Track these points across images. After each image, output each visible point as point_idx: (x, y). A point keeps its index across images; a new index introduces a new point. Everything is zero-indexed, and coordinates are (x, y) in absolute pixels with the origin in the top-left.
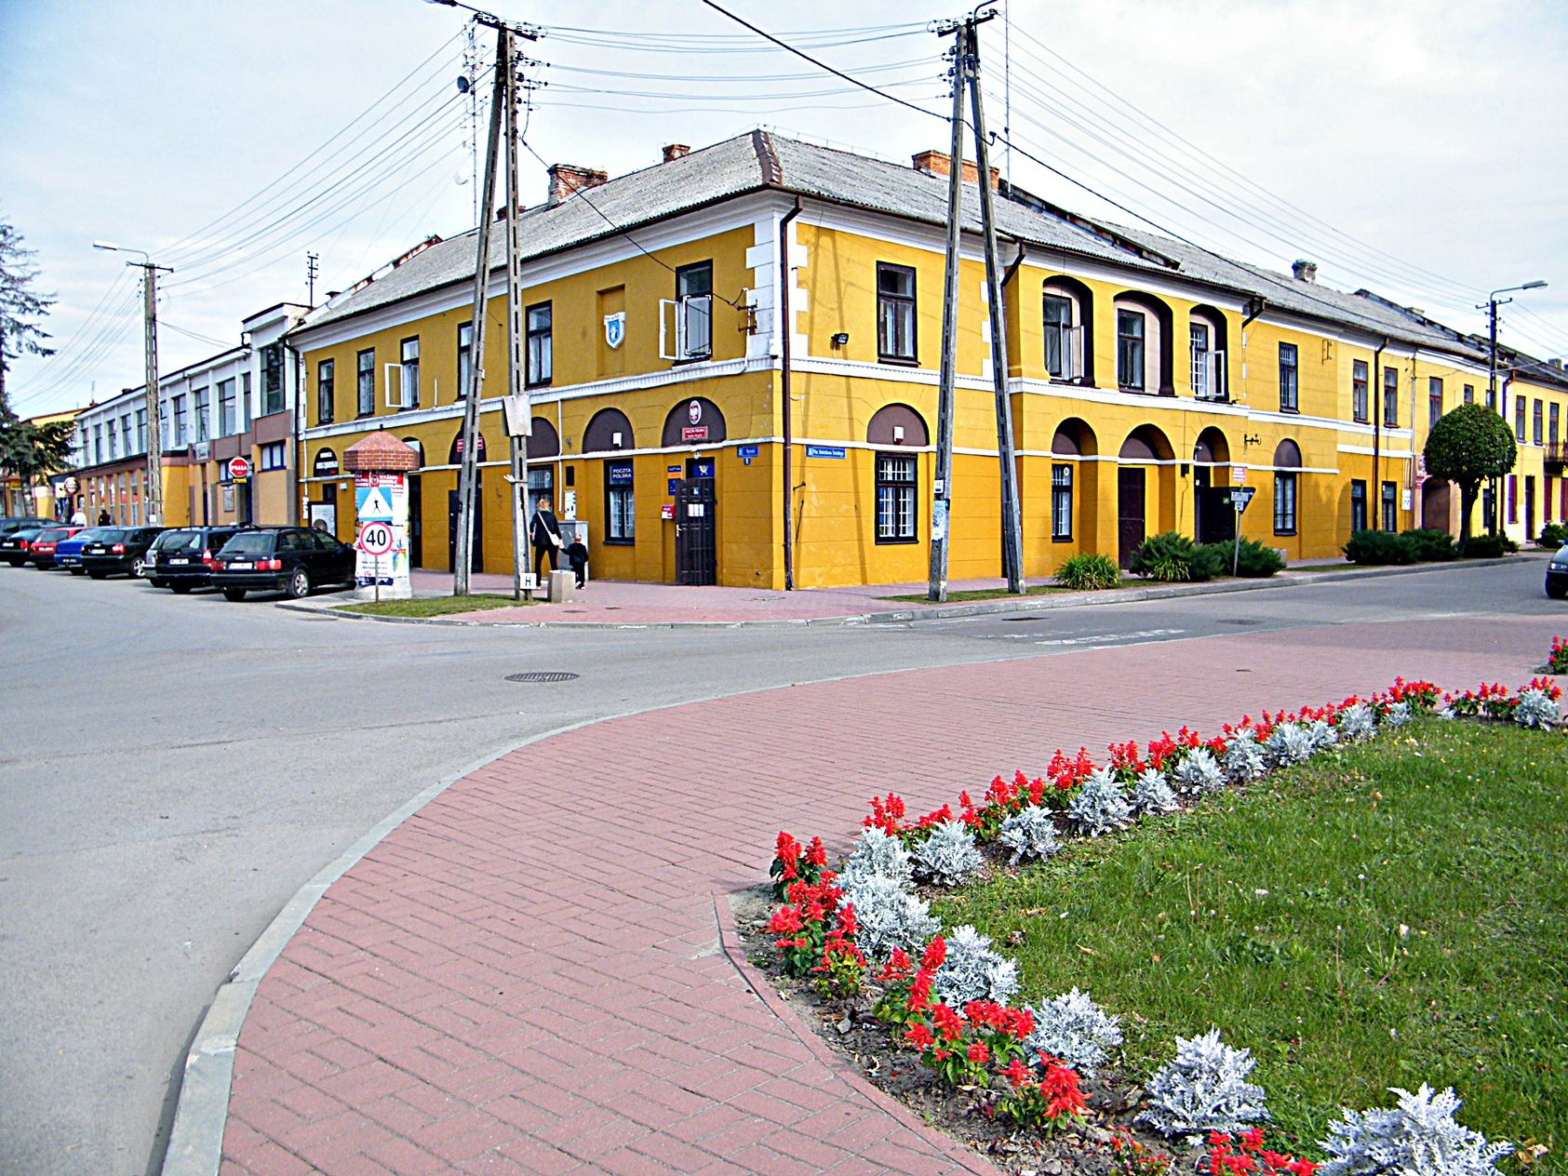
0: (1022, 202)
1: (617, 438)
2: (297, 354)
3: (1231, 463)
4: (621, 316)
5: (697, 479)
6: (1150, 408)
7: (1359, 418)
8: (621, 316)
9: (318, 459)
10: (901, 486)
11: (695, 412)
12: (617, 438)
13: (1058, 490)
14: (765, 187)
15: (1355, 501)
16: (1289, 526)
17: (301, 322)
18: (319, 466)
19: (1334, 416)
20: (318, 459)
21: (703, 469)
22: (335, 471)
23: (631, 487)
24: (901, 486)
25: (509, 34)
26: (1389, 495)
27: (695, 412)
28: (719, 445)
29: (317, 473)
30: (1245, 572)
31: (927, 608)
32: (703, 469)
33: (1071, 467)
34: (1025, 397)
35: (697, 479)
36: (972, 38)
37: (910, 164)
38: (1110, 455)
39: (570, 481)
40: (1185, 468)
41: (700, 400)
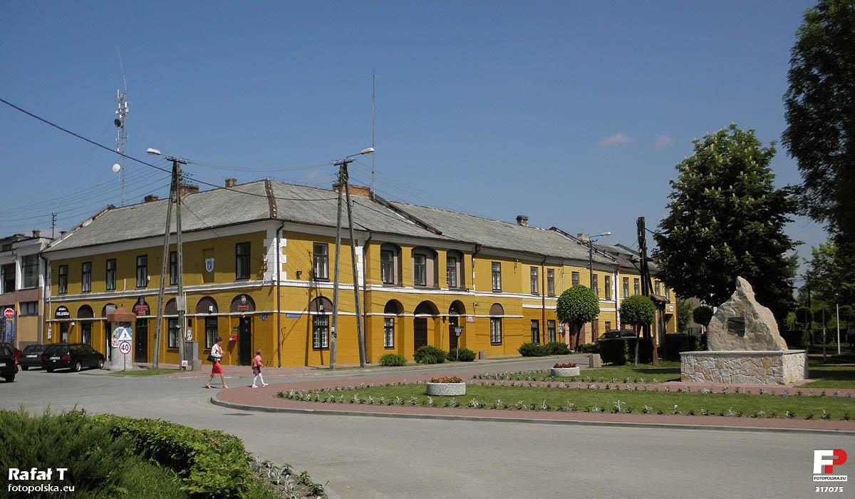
0: (380, 203)
1: (211, 308)
2: (46, 261)
3: (230, 365)
4: (213, 260)
5: (245, 326)
6: (427, 294)
7: (535, 293)
8: (213, 260)
9: (58, 311)
10: (322, 328)
11: (244, 299)
12: (211, 308)
13: (388, 328)
14: (271, 219)
15: (533, 329)
16: (499, 341)
17: (48, 246)
18: (59, 314)
19: (519, 291)
20: (58, 311)
21: (246, 322)
22: (68, 317)
23: (217, 328)
24: (322, 328)
25: (178, 163)
26: (552, 326)
27: (244, 299)
28: (253, 313)
29: (57, 317)
30: (462, 360)
31: (329, 372)
32: (246, 322)
33: (394, 319)
34: (373, 294)
35: (245, 326)
36: (345, 168)
37: (331, 188)
38: (409, 315)
39: (190, 324)
40: (444, 317)
41: (246, 296)
